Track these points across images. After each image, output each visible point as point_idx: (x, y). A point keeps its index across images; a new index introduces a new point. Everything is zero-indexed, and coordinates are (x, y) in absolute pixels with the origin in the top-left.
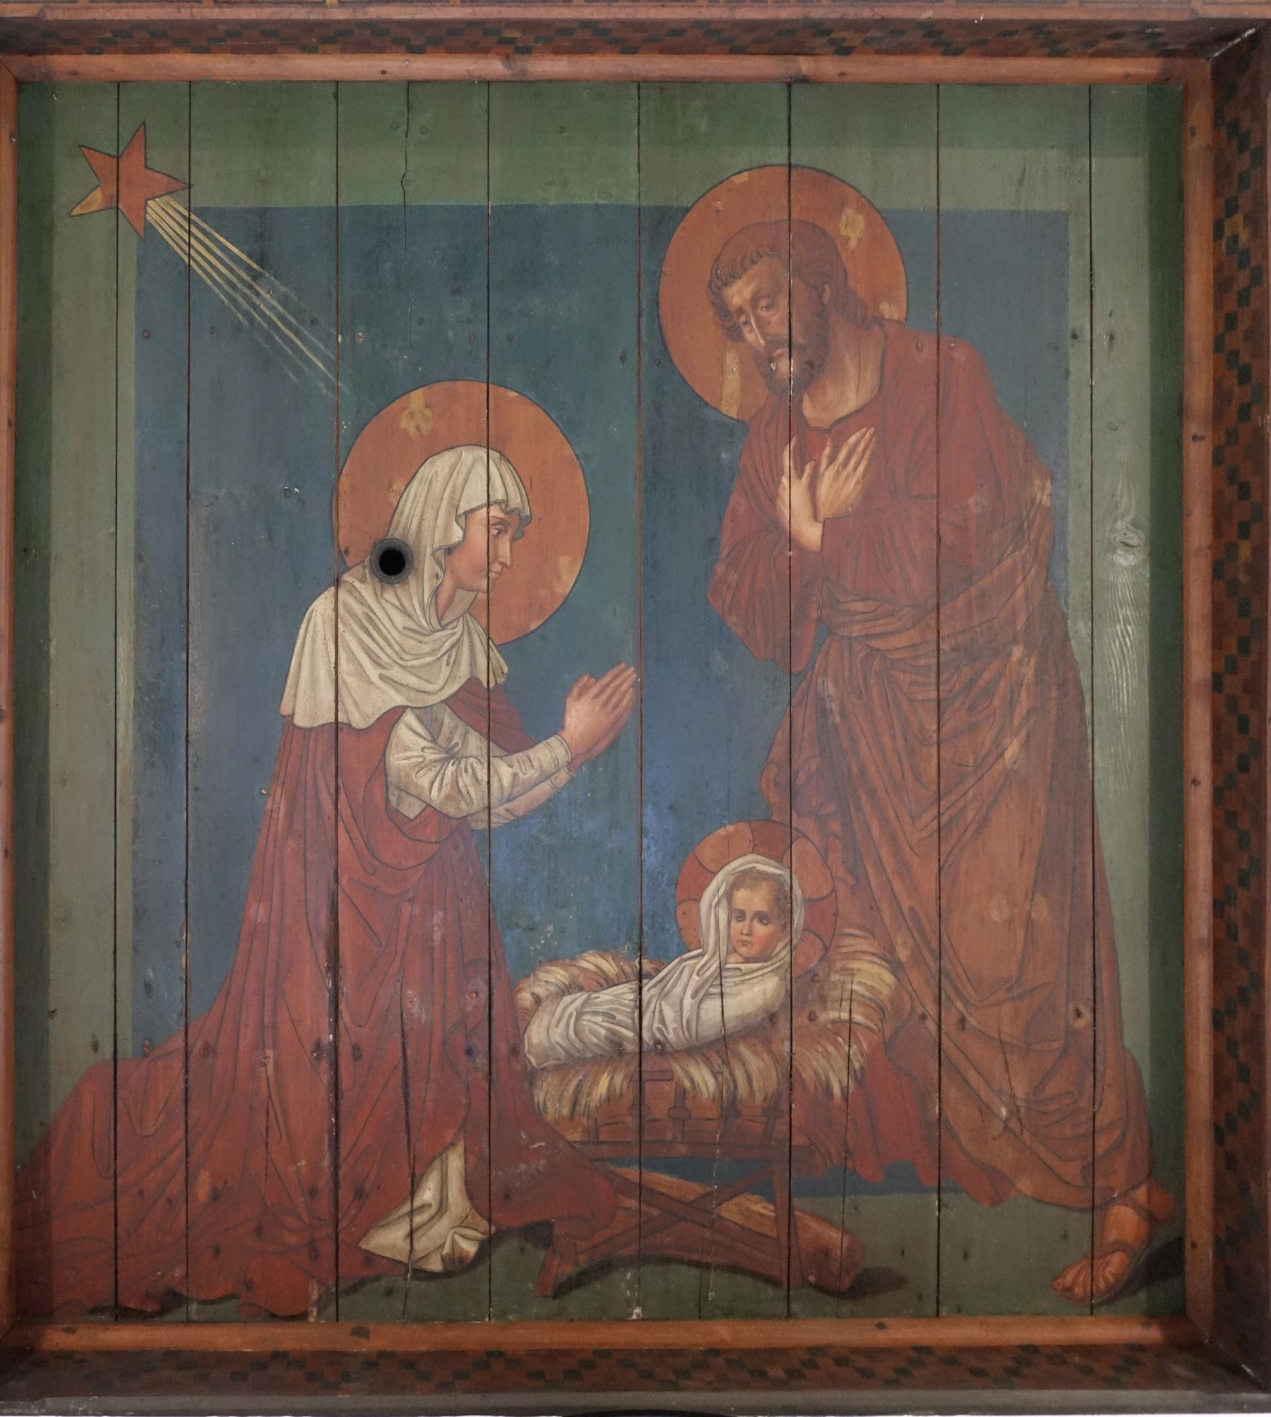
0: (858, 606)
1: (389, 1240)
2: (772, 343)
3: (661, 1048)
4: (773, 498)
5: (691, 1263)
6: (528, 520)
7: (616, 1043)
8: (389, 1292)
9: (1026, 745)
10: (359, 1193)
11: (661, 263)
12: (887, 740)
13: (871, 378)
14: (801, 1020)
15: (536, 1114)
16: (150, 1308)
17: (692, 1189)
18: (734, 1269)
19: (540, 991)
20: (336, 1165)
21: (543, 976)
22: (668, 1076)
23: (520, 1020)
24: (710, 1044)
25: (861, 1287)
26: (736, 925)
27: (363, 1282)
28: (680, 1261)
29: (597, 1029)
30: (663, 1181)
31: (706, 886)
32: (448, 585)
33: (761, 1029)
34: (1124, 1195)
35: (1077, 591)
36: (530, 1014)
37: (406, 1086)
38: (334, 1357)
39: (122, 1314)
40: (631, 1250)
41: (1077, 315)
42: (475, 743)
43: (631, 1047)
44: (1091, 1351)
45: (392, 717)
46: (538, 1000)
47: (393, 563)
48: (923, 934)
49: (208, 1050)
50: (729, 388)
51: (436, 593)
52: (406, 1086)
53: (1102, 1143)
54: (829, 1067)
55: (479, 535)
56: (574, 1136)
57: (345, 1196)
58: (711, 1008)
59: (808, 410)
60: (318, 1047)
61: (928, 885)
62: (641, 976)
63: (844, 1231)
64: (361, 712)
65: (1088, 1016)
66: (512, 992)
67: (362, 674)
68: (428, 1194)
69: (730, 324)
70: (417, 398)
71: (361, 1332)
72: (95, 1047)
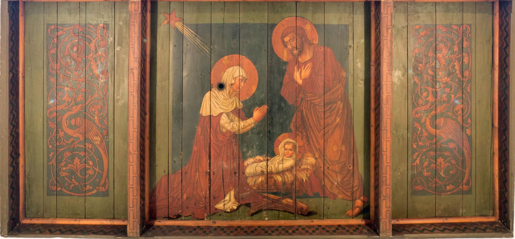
0: (309, 95)
1: (220, 206)
2: (293, 48)
3: (272, 173)
4: (293, 75)
5: (277, 210)
6: (246, 79)
7: (262, 172)
8: (220, 215)
9: (341, 119)
10: (214, 198)
11: (272, 33)
12: (314, 118)
13: (311, 54)
14: (298, 168)
15: (248, 184)
16: (175, 217)
17: (276, 197)
18: (285, 211)
19: (248, 163)
20: (210, 193)
21: (249, 160)
22: (273, 178)
23: (245, 168)
24: (281, 172)
25: (309, 214)
26: (286, 151)
27: (215, 213)
28: (275, 210)
29: (259, 169)
30: (272, 196)
31: (280, 144)
32: (232, 91)
33: (290, 170)
34: (359, 198)
35: (350, 91)
36: (246, 167)
37: (223, 179)
38: (209, 227)
39: (169, 218)
40: (266, 208)
41: (350, 43)
42: (237, 119)
43: (266, 173)
44: (350, 226)
45: (221, 114)
46: (248, 164)
47: (221, 86)
48: (321, 153)
49: (186, 173)
50: (285, 56)
51: (229, 92)
52: (223, 179)
53: (355, 189)
54: (303, 176)
55: (237, 82)
56: (255, 188)
57: (212, 198)
58: (281, 166)
59: (300, 59)
60: (206, 172)
61: (322, 144)
62: (267, 160)
63: (306, 204)
64: (215, 114)
65: (352, 167)
66: (243, 162)
67: (215, 107)
68: (227, 198)
69: (285, 45)
70: (226, 57)
71: (214, 222)
72: (165, 172)
